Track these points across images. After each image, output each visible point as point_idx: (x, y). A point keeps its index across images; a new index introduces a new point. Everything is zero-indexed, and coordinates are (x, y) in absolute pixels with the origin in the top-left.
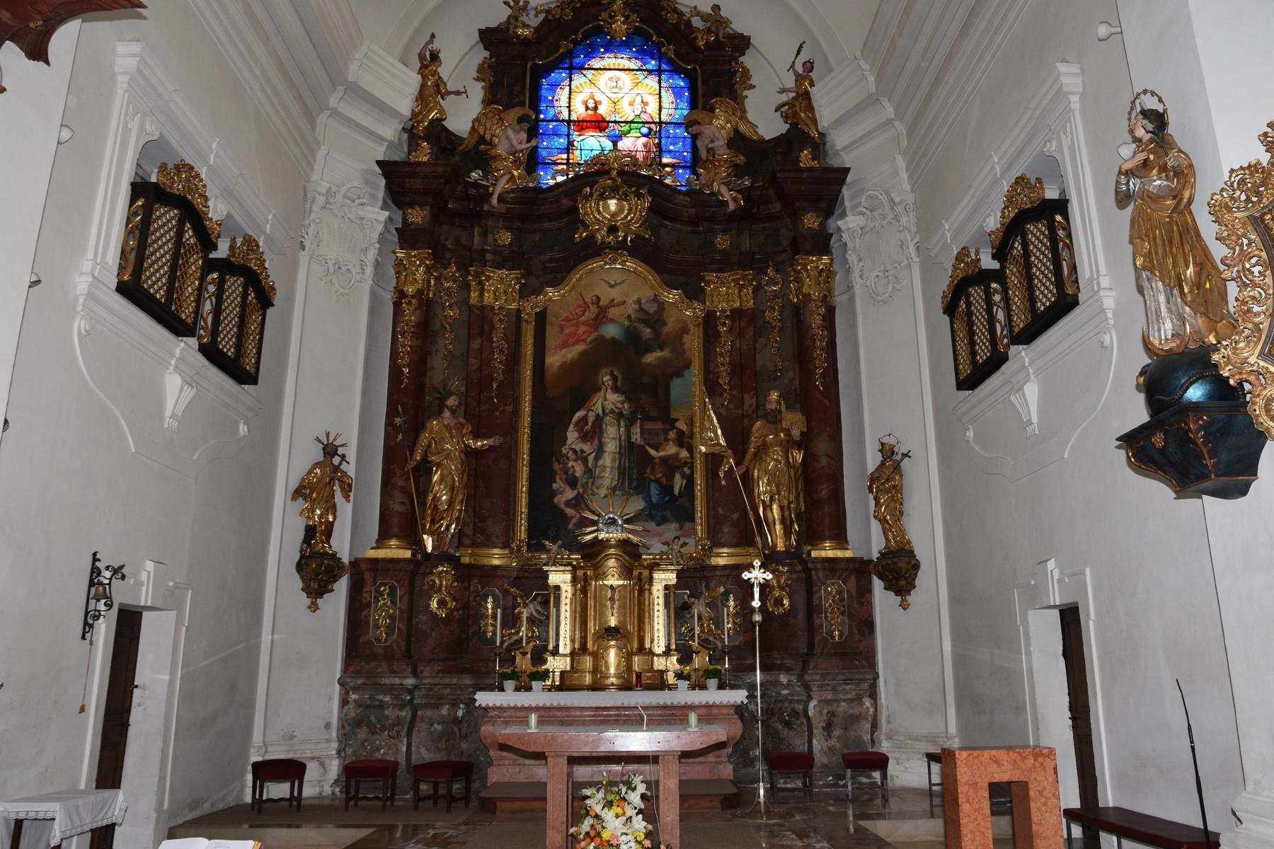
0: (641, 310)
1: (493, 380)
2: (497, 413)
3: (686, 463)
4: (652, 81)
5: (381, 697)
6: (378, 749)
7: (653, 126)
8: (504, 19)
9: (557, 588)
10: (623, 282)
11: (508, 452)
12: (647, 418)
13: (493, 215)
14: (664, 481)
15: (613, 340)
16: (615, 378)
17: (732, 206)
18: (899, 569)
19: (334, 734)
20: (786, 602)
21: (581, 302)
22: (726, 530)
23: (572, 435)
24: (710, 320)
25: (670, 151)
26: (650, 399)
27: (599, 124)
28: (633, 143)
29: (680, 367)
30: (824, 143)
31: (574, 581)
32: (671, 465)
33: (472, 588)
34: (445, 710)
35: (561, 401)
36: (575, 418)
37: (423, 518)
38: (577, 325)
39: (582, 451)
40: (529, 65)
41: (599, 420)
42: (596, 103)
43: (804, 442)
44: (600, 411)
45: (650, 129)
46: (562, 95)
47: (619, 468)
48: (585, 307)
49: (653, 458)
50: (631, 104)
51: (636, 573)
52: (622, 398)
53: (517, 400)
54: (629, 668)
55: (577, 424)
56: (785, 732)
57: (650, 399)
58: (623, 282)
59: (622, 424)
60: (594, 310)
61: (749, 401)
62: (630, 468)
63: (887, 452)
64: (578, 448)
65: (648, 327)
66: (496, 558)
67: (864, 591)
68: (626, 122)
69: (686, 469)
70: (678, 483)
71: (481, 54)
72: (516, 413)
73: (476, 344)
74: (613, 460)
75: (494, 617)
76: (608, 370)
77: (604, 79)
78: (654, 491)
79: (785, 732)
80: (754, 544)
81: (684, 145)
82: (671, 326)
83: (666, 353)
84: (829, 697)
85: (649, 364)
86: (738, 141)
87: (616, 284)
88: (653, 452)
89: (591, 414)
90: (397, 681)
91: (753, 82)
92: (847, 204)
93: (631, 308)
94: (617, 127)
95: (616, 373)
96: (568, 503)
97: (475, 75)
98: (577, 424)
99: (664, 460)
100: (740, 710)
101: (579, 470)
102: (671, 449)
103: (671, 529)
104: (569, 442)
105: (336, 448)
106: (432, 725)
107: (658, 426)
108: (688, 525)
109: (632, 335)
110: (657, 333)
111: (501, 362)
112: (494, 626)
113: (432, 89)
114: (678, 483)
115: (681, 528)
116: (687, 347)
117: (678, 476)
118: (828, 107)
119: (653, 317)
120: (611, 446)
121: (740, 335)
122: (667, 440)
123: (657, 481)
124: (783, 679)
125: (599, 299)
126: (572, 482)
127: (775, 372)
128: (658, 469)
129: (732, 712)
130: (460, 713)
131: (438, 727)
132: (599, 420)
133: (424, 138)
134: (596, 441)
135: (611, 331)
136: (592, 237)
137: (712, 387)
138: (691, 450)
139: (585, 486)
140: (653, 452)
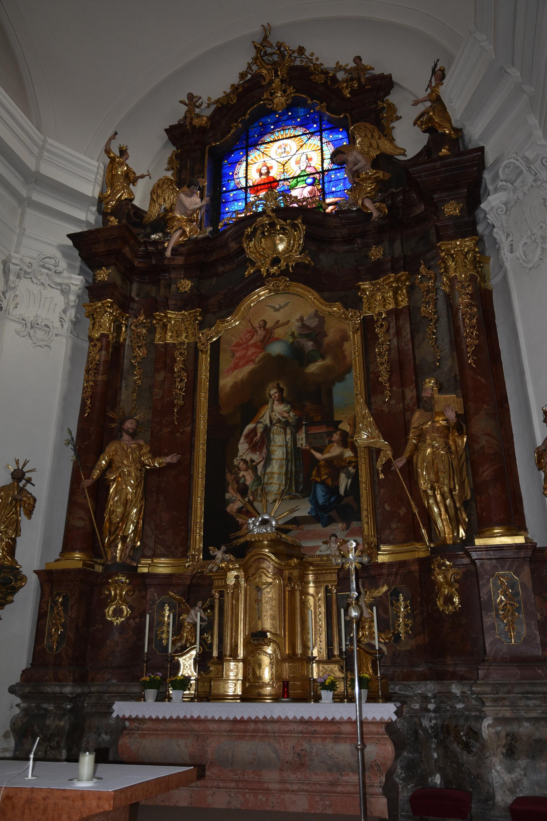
0: (304, 326)
1: (174, 406)
2: (178, 435)
3: (350, 463)
4: (315, 141)
5: (45, 706)
7: (317, 176)
8: (181, 115)
10: (286, 305)
11: (185, 467)
12: (312, 423)
13: (174, 268)
14: (329, 482)
16: (281, 390)
17: (375, 214)
20: (456, 600)
21: (250, 328)
23: (243, 446)
24: (368, 325)
25: (333, 192)
26: (314, 405)
28: (301, 192)
29: (341, 372)
30: (462, 136)
32: (335, 466)
33: (149, 596)
35: (233, 418)
36: (246, 431)
37: (101, 533)
38: (247, 348)
39: (252, 461)
40: (207, 148)
41: (267, 430)
42: (268, 169)
43: (462, 424)
44: (268, 422)
45: (314, 179)
46: (241, 170)
47: (286, 474)
48: (254, 331)
49: (318, 461)
50: (298, 162)
52: (287, 408)
53: (194, 421)
55: (247, 437)
56: (465, 757)
57: (314, 405)
58: (286, 305)
59: (288, 431)
61: (410, 393)
62: (297, 473)
64: (248, 459)
65: (310, 340)
68: (293, 178)
69: (351, 470)
70: (344, 482)
71: (171, 149)
72: (193, 433)
73: (160, 377)
74: (281, 466)
75: (169, 624)
76: (275, 384)
77: (273, 150)
78: (320, 492)
79: (465, 757)
80: (420, 539)
81: (344, 185)
83: (328, 361)
84: (508, 714)
85: (313, 374)
86: (382, 161)
87: (281, 307)
88: (318, 455)
89: (260, 425)
90: (57, 689)
91: (399, 114)
92: (490, 187)
93: (295, 326)
94: (286, 183)
95: (281, 386)
97: (166, 166)
98: (247, 437)
99: (329, 461)
101: (248, 477)
102: (335, 451)
104: (240, 453)
105: (24, 474)
106: (99, 735)
107: (323, 429)
108: (355, 524)
110: (318, 344)
111: (181, 389)
113: (118, 173)
114: (344, 482)
115: (348, 527)
116: (347, 353)
117: (343, 476)
118: (456, 99)
119: (314, 332)
120: (278, 453)
121: (398, 333)
122: (331, 442)
123: (323, 483)
124: (456, 689)
125: (265, 322)
126: (243, 490)
127: (435, 362)
128: (324, 471)
129: (383, 730)
132: (267, 430)
133: (112, 214)
134: (265, 450)
135: (277, 349)
137: (372, 388)
139: (254, 494)
140: (318, 455)
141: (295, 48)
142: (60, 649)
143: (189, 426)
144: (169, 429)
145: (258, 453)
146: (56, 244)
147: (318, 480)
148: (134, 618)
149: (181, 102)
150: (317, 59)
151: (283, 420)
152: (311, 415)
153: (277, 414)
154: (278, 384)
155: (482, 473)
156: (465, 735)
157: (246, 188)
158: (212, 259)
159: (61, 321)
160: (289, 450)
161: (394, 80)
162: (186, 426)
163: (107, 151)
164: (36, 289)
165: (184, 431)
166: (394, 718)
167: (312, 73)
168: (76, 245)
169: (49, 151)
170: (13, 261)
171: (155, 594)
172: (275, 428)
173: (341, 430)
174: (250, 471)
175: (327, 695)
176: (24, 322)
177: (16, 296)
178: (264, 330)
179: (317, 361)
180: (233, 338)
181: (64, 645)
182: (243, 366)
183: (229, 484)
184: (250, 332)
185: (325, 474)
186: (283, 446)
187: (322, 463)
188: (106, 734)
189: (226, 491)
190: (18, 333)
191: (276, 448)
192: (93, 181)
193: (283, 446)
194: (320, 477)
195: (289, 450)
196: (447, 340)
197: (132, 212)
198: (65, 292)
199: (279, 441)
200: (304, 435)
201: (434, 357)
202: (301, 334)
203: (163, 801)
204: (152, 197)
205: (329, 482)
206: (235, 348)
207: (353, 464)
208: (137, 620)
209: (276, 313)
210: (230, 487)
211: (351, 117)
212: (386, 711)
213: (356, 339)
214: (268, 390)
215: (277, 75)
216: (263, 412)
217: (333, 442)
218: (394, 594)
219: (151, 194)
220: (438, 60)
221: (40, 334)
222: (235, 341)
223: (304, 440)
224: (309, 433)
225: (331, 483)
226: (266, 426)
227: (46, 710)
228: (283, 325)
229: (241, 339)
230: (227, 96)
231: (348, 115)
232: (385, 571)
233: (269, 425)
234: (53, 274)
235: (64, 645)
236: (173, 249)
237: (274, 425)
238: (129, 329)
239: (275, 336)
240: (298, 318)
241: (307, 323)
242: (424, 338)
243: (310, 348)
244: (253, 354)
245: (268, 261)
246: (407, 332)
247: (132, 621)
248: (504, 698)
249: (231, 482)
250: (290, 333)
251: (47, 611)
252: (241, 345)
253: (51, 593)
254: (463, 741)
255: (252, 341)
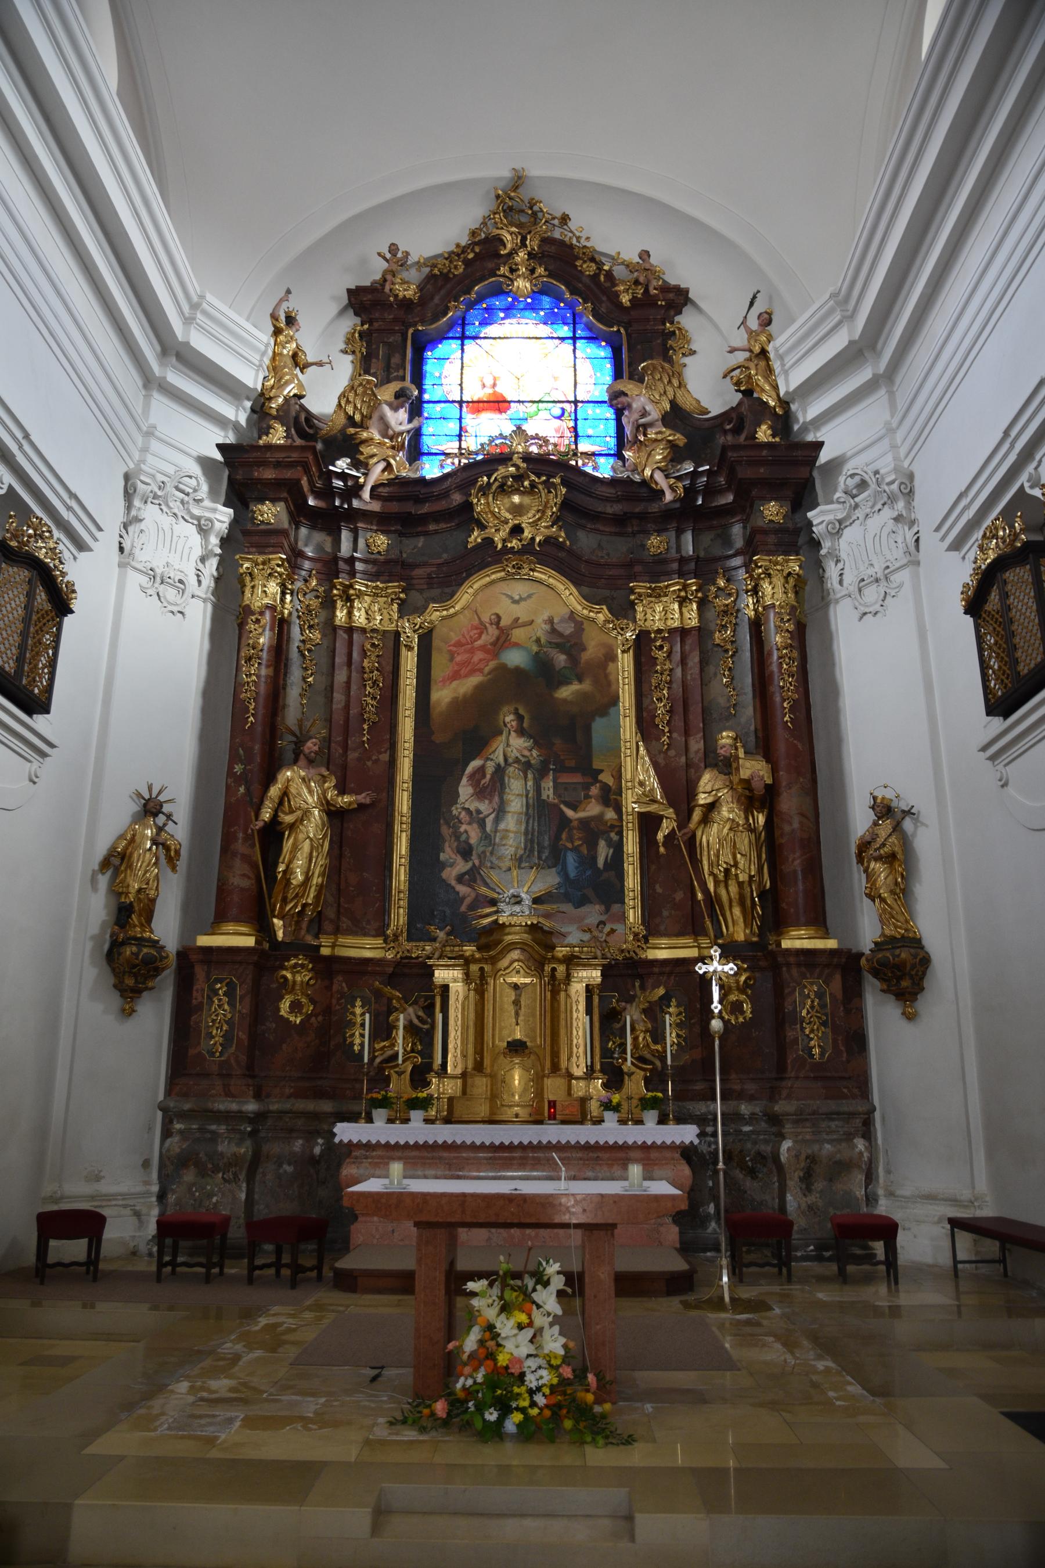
0: (554, 631)
2: (369, 763)
3: (612, 827)
5: (214, 1127)
6: (210, 1196)
7: (567, 406)
9: (445, 988)
10: (529, 596)
12: (562, 769)
15: (518, 671)
16: (520, 718)
17: (669, 496)
18: (904, 969)
19: (155, 1175)
21: (476, 622)
22: (665, 913)
23: (465, 790)
24: (643, 643)
26: (569, 743)
27: (499, 404)
31: (467, 978)
32: (592, 831)
33: (335, 987)
34: (298, 1145)
38: (472, 651)
39: (479, 812)
41: (500, 772)
42: (495, 379)
44: (501, 760)
47: (526, 833)
48: (481, 628)
51: (548, 968)
52: (529, 743)
54: (539, 1093)
55: (471, 777)
56: (748, 1184)
58: (529, 596)
59: (530, 776)
60: (493, 631)
63: (884, 810)
64: (472, 808)
65: (563, 652)
66: (365, 948)
67: (853, 994)
69: (613, 836)
70: (603, 852)
71: (350, 323)
74: (519, 822)
75: (363, 1025)
76: (512, 709)
78: (571, 860)
82: (592, 651)
83: (586, 686)
85: (565, 701)
86: (675, 415)
87: (521, 599)
88: (570, 813)
89: (489, 764)
90: (234, 1107)
91: (694, 347)
93: (540, 629)
94: (521, 407)
95: (521, 711)
96: (460, 879)
99: (585, 823)
100: (687, 1152)
101: (474, 835)
102: (593, 809)
103: (593, 913)
104: (462, 799)
106: (280, 1166)
107: (577, 778)
108: (616, 908)
109: (542, 665)
110: (573, 659)
112: (362, 1036)
114: (603, 852)
117: (602, 844)
119: (568, 640)
121: (683, 661)
122: (587, 797)
123: (576, 849)
125: (499, 617)
126: (466, 852)
127: (729, 708)
128: (577, 834)
130: (317, 1150)
131: (289, 1169)
132: (500, 772)
134: (496, 799)
135: (515, 658)
136: (489, 542)
138: (618, 809)
139: (482, 856)
140: (570, 813)
141: (558, 215)
142: (226, 1055)
143: (385, 752)
144: (357, 755)
145: (487, 802)
146: (195, 454)
147: (569, 845)
148: (316, 1016)
149: (379, 254)
150: (588, 238)
151: (523, 760)
152: (562, 757)
153: (515, 751)
154: (517, 709)
155: (793, 862)
156: (751, 1160)
157: (461, 403)
158: (422, 512)
159: (198, 576)
160: (531, 801)
161: (690, 295)
162: (380, 753)
163: (274, 317)
164: (166, 521)
165: (377, 761)
166: (696, 1141)
167: (578, 258)
168: (228, 462)
169: (205, 313)
170: (143, 478)
171: (344, 985)
172: (511, 769)
173: (601, 782)
174: (475, 826)
175: (610, 1117)
176: (182, 586)
177: (142, 531)
178: (498, 628)
179: (571, 683)
180: (452, 634)
181: (233, 1049)
182: (466, 676)
183: (444, 841)
184: (477, 628)
185: (579, 839)
186: (522, 795)
187: (575, 824)
188: (289, 1164)
189: (440, 849)
190: (143, 590)
191: (512, 798)
192: (257, 363)
193: (522, 795)
194: (572, 843)
195: (531, 801)
196: (749, 680)
197: (303, 416)
198: (203, 531)
199: (516, 787)
200: (551, 784)
201: (729, 701)
202: (550, 643)
203: (402, 1240)
204: (339, 402)
205: (584, 850)
206: (454, 649)
207: (616, 830)
208: (320, 1018)
209: (515, 606)
210: (447, 844)
211: (628, 335)
212: (687, 1134)
213: (625, 663)
214: (502, 717)
215: (523, 245)
216: (494, 746)
217: (591, 797)
218: (665, 1000)
219: (339, 399)
220: (758, 292)
221: (170, 594)
222: (454, 637)
223: (552, 790)
224: (559, 781)
225: (586, 852)
226: (499, 765)
227: (213, 1132)
228: (524, 625)
229: (463, 635)
230: (450, 257)
231: (622, 330)
232: (656, 970)
233: (502, 763)
234: (191, 502)
235: (233, 1049)
236: (373, 489)
237: (510, 765)
238: (295, 597)
239: (513, 640)
240: (546, 618)
241: (559, 628)
242: (715, 674)
243: (563, 664)
244: (481, 660)
245: (507, 528)
246: (694, 659)
247: (313, 1019)
248: (807, 1120)
249: (447, 837)
250: (534, 638)
251: (202, 1003)
252: (463, 645)
253: (208, 978)
254: (748, 1167)
255: (479, 643)
